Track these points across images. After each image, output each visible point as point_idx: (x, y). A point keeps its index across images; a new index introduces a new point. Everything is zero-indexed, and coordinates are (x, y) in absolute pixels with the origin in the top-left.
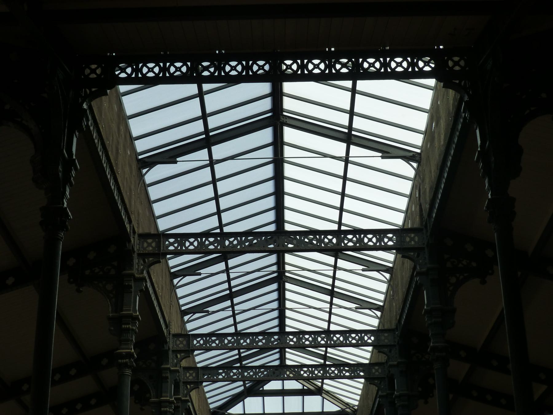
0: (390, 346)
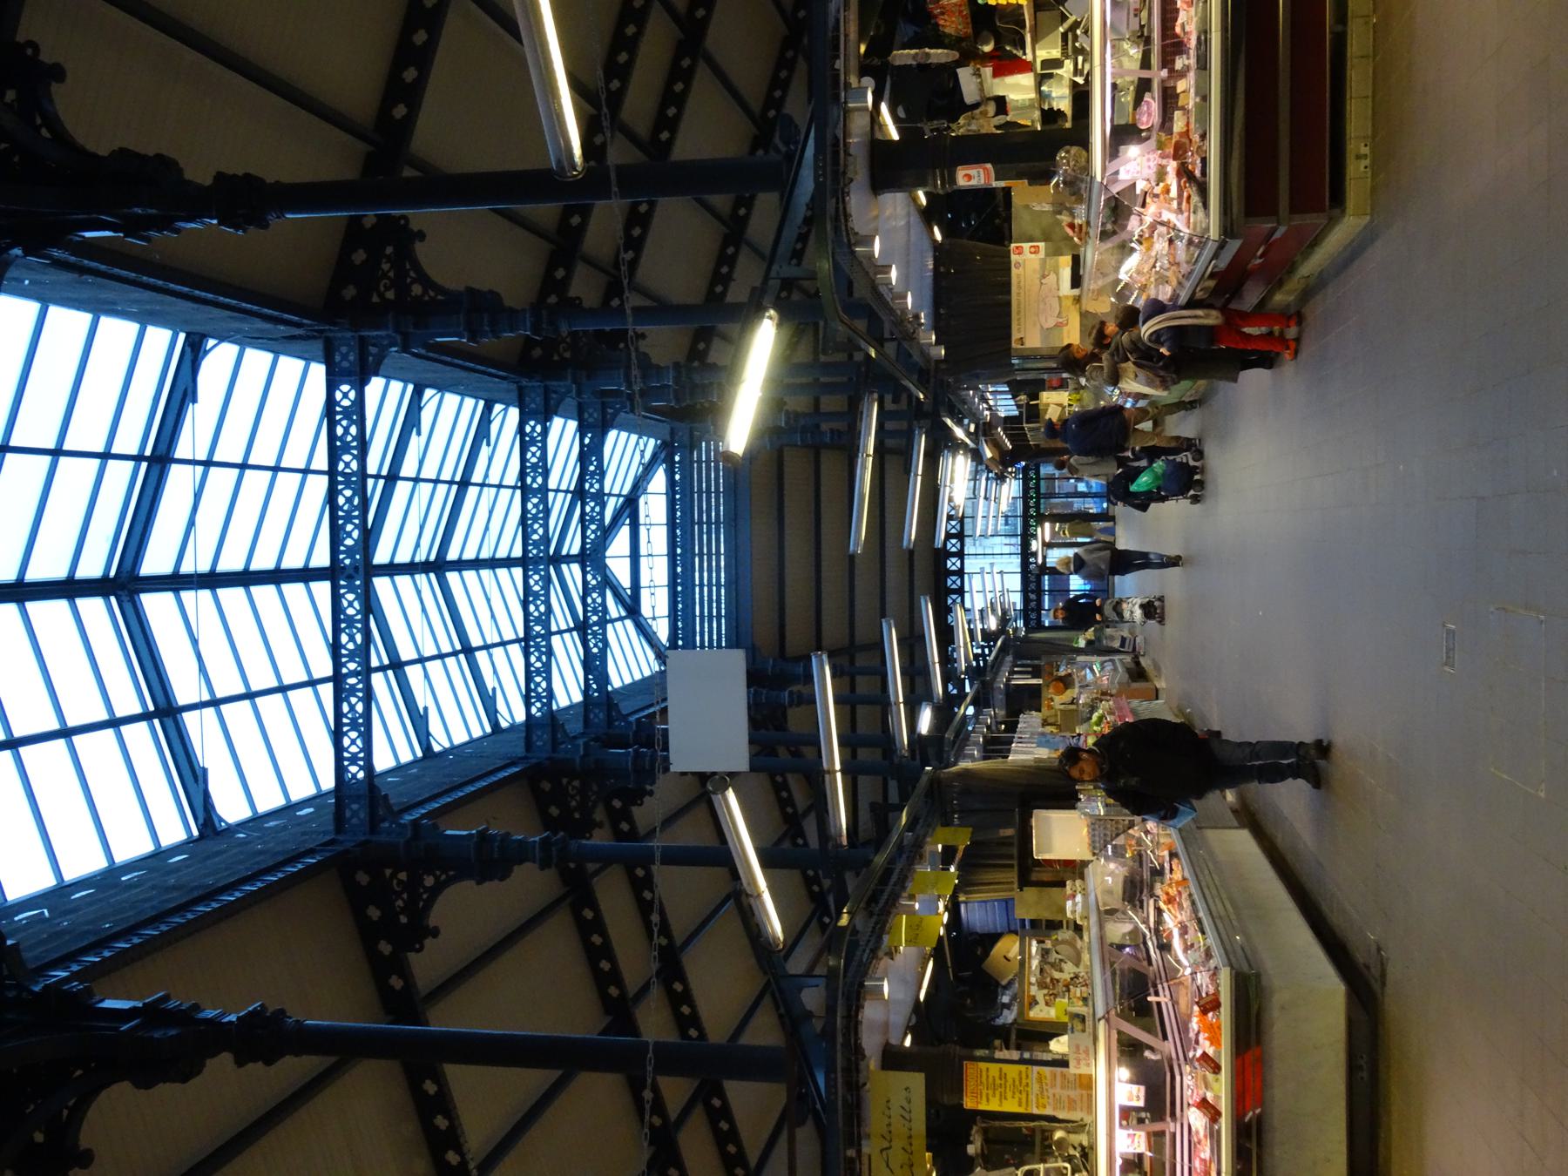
0: (547, 392)
